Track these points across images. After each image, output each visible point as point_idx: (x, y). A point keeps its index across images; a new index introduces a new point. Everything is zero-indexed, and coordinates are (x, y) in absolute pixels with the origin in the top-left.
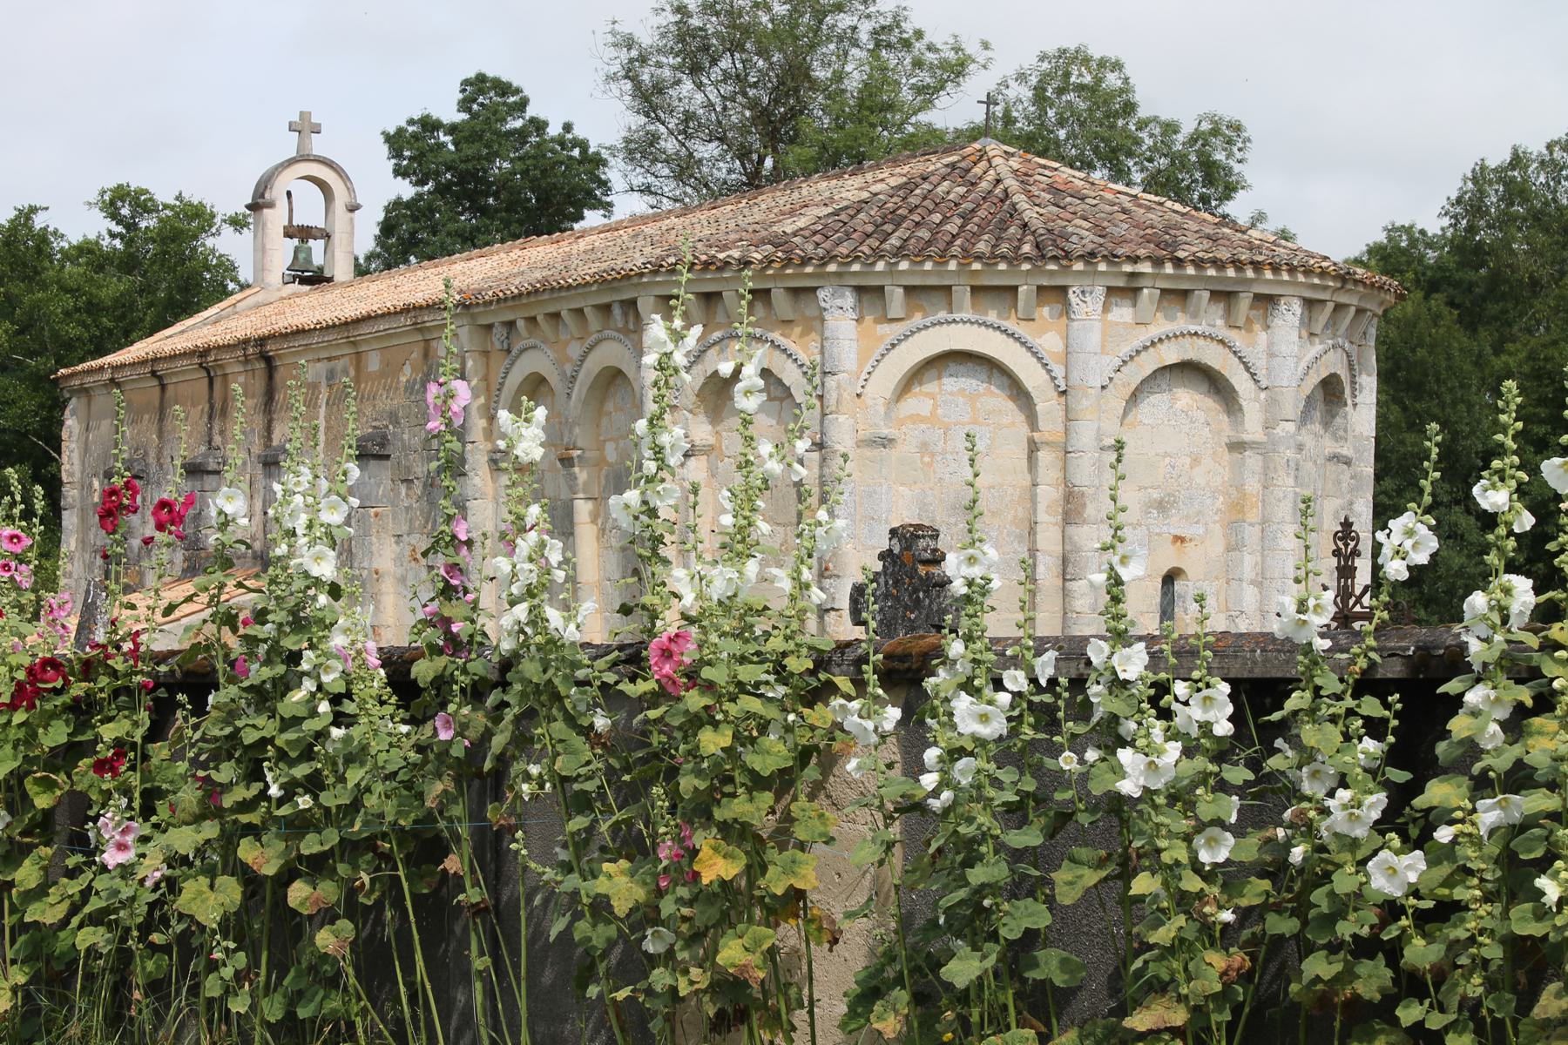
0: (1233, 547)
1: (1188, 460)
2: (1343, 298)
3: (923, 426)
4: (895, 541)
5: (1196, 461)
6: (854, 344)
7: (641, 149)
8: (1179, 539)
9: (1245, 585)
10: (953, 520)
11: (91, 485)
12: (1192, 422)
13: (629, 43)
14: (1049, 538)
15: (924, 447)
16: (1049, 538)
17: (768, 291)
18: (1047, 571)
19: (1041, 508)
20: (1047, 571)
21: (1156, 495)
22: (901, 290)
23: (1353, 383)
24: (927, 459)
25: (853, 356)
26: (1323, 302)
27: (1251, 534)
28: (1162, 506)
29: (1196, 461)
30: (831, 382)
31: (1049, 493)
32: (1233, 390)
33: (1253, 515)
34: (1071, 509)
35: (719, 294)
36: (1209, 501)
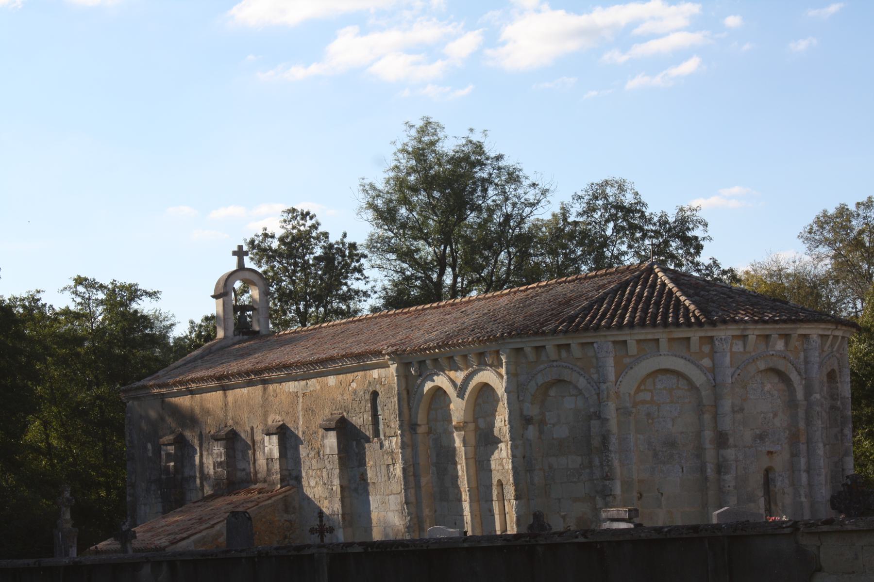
0: (794, 455)
1: (772, 415)
2: (837, 333)
3: (647, 406)
4: (848, 480)
5: (775, 415)
6: (613, 369)
7: (377, 245)
8: (770, 453)
9: (802, 473)
10: (664, 449)
11: (145, 448)
12: (772, 396)
13: (373, 187)
14: (710, 454)
15: (648, 415)
16: (710, 454)
17: (569, 345)
18: (710, 470)
19: (406, 400)
20: (710, 470)
21: (758, 432)
22: (635, 342)
23: (840, 372)
24: (650, 421)
25: (613, 374)
26: (828, 336)
27: (803, 448)
28: (761, 437)
29: (775, 415)
30: (603, 387)
31: (708, 434)
32: (791, 380)
33: (803, 439)
34: (722, 440)
35: (544, 347)
36: (782, 434)
